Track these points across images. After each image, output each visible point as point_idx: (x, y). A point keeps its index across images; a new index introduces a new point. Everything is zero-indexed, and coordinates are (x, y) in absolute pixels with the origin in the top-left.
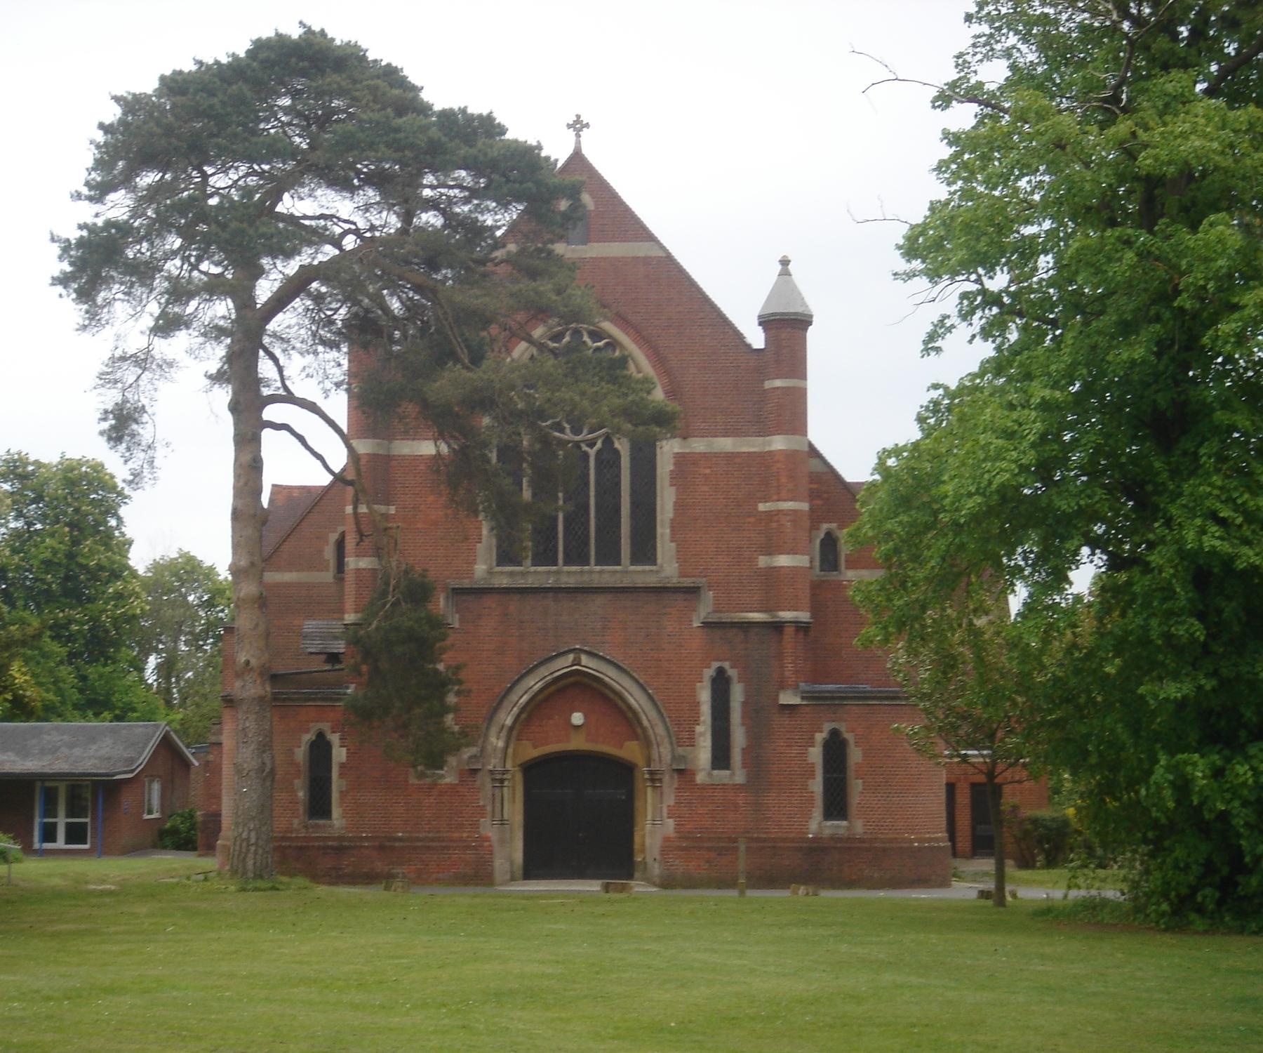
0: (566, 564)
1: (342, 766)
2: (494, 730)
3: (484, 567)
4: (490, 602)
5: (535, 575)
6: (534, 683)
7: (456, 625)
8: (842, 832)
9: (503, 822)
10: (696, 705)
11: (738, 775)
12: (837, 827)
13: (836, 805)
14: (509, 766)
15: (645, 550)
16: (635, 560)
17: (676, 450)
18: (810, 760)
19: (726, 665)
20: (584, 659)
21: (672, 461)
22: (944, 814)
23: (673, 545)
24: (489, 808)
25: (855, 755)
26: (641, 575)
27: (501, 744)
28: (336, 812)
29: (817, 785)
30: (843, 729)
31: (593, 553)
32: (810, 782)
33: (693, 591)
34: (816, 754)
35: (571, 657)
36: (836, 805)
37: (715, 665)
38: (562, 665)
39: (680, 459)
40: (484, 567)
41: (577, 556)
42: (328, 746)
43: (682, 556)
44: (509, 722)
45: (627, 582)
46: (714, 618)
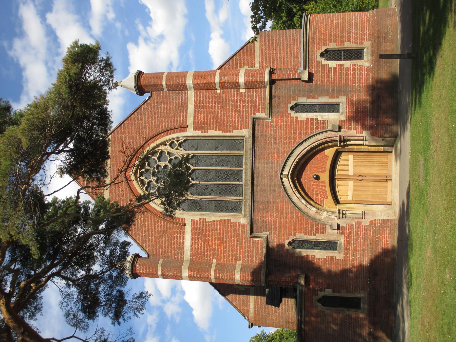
0: (242, 181)
1: (334, 291)
2: (318, 217)
3: (242, 219)
4: (257, 217)
5: (245, 197)
6: (296, 197)
7: (268, 233)
8: (370, 52)
9: (364, 214)
10: (309, 120)
11: (342, 100)
12: (367, 54)
13: (356, 54)
14: (336, 210)
15: (235, 143)
16: (240, 180)
17: (192, 130)
18: (334, 66)
19: (290, 106)
20: (285, 172)
21: (197, 132)
22: (315, 158)
23: (234, 131)
24: (356, 220)
25: (333, 46)
26: (247, 146)
27: (325, 213)
28: (358, 295)
29: (347, 63)
30: (321, 52)
31: (238, 198)
32: (345, 66)
33: (254, 121)
34: (333, 64)
35: (284, 179)
36: (356, 54)
37: (289, 111)
38: (287, 182)
39: (196, 128)
40: (242, 219)
41: (237, 175)
42: (324, 297)
43: (239, 128)
44: (314, 209)
45: (250, 152)
46: (267, 112)
